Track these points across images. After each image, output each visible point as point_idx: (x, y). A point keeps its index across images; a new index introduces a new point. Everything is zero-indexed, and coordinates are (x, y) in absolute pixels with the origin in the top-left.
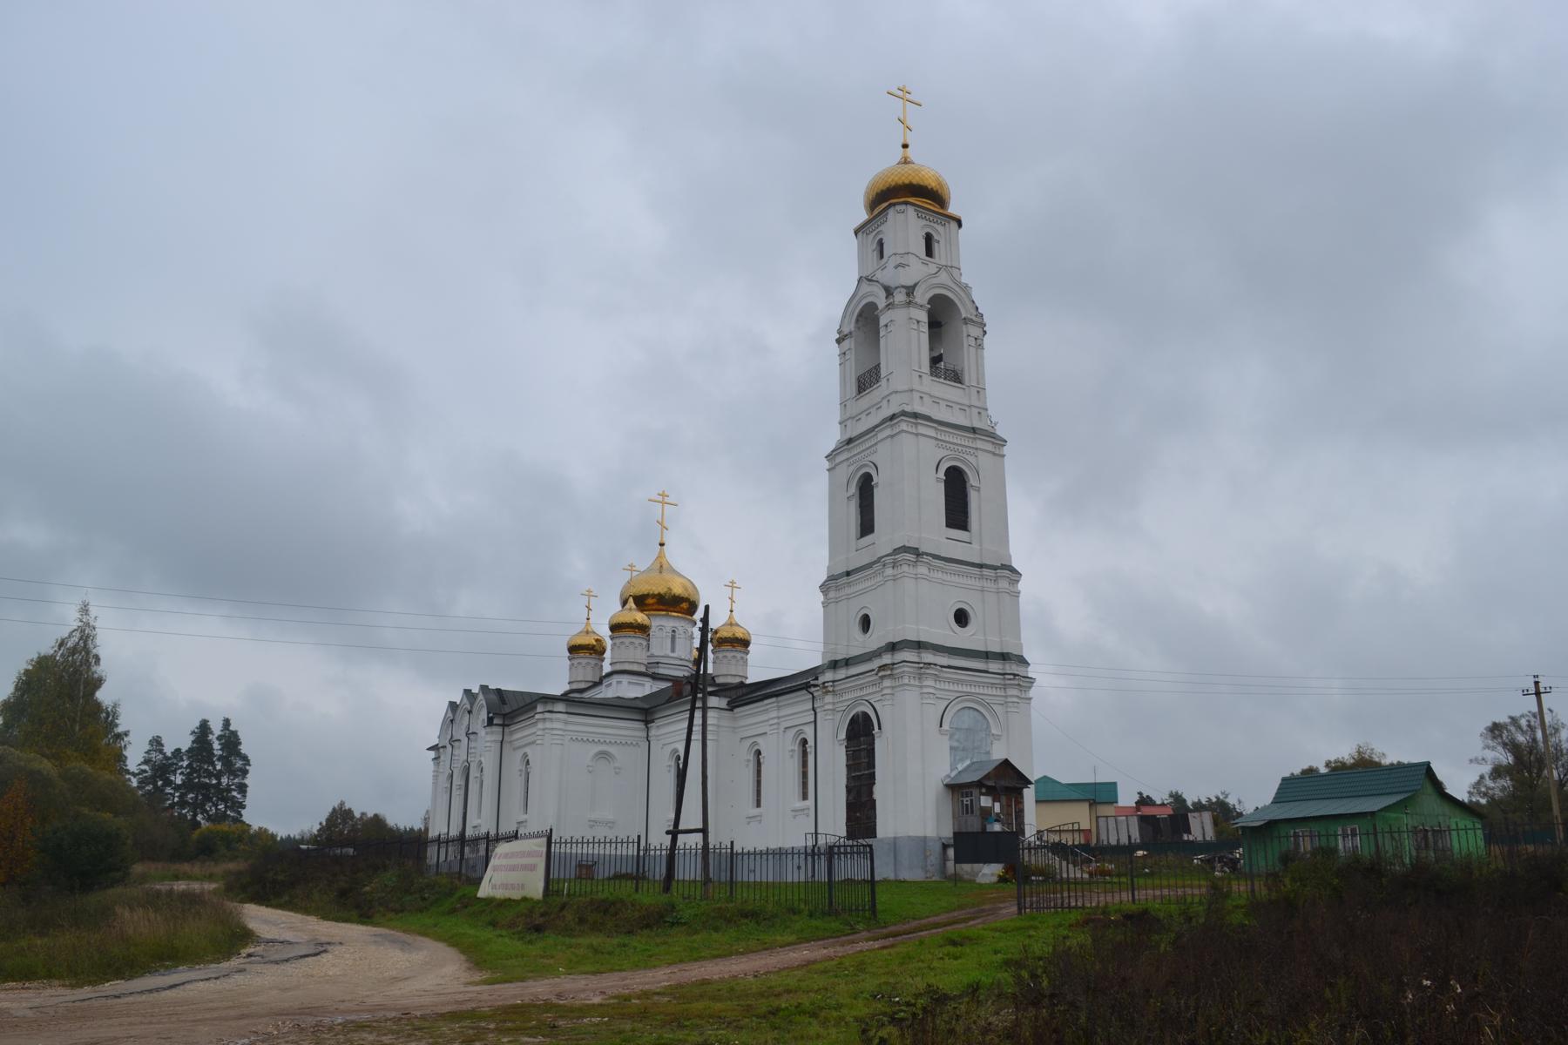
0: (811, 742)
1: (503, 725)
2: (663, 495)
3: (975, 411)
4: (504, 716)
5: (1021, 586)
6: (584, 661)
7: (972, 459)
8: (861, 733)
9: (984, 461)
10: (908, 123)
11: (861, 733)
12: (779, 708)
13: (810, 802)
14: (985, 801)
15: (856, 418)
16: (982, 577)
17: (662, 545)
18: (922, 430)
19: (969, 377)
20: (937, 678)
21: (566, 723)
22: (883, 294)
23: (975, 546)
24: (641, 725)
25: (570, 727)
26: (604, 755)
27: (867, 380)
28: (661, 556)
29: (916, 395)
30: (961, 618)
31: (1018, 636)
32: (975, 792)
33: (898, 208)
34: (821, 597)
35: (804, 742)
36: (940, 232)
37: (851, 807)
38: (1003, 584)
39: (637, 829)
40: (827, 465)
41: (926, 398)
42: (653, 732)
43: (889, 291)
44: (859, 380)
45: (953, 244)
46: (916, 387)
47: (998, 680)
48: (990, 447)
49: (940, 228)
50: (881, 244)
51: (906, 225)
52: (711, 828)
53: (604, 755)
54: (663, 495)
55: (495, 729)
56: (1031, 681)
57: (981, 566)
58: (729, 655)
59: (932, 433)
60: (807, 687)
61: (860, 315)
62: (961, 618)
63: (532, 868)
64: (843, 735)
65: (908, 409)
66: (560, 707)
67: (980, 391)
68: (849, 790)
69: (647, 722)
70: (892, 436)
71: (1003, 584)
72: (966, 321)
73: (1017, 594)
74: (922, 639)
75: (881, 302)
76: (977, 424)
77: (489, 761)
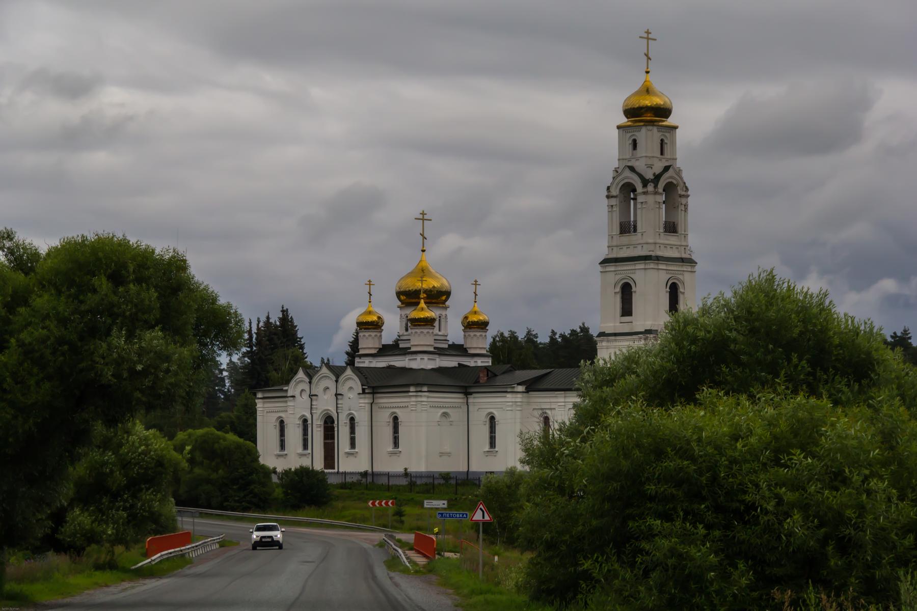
0: (310, 422)
4: (373, 388)
7: (681, 277)
9: (687, 278)
12: (565, 397)
13: (309, 451)
15: (620, 247)
18: (661, 267)
19: (680, 229)
21: (428, 397)
26: (445, 415)
27: (627, 228)
29: (658, 246)
31: (501, 472)
35: (305, 421)
37: (325, 444)
40: (599, 268)
42: (470, 400)
44: (621, 224)
45: (673, 142)
46: (658, 241)
50: (673, 304)
51: (648, 137)
55: (367, 396)
58: (478, 334)
61: (623, 185)
65: (653, 254)
70: (645, 269)
76: (684, 256)
77: (362, 419)
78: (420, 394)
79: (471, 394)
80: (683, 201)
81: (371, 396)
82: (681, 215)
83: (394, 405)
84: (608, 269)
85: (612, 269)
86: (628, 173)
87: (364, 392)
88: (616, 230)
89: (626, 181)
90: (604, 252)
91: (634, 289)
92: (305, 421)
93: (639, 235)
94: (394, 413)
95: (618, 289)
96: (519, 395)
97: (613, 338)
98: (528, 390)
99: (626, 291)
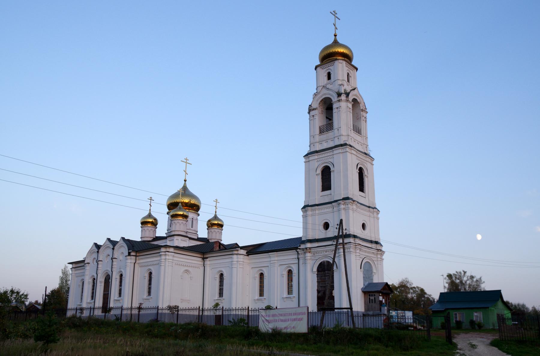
0: (295, 272)
1: (136, 256)
2: (186, 159)
3: (365, 146)
5: (379, 216)
6: (150, 228)
8: (325, 271)
9: (368, 165)
10: (337, 26)
11: (325, 271)
14: (381, 298)
16: (369, 211)
17: (185, 181)
20: (360, 250)
22: (335, 96)
23: (367, 199)
24: (200, 259)
25: (175, 259)
26: (187, 271)
28: (185, 183)
30: (364, 226)
31: (379, 235)
32: (376, 294)
33: (340, 61)
34: (302, 213)
35: (290, 272)
36: (352, 73)
37: (104, 295)
38: (375, 214)
39: (198, 304)
40: (304, 160)
41: (353, 140)
43: (339, 95)
47: (375, 251)
48: (370, 160)
49: (351, 71)
52: (353, 307)
53: (187, 271)
54: (186, 159)
56: (384, 252)
57: (369, 207)
58: (216, 230)
59: (355, 153)
60: (296, 249)
61: (322, 100)
62: (364, 226)
63: (301, 320)
64: (315, 269)
66: (172, 250)
67: (367, 138)
68: (318, 292)
69: (204, 259)
71: (375, 214)
72: (362, 110)
73: (378, 219)
74: (355, 234)
75: (334, 98)
78: (167, 253)
79: (207, 258)
80: (363, 114)
81: (134, 257)
82: (363, 123)
83: (150, 263)
84: (311, 158)
85: (316, 157)
86: (325, 91)
87: (129, 254)
88: (317, 131)
89: (324, 97)
90: (307, 150)
91: (332, 169)
92: (290, 272)
93: (336, 131)
94: (221, 271)
95: (319, 171)
96: (242, 257)
97: (317, 207)
98: (248, 254)
99: (326, 173)
